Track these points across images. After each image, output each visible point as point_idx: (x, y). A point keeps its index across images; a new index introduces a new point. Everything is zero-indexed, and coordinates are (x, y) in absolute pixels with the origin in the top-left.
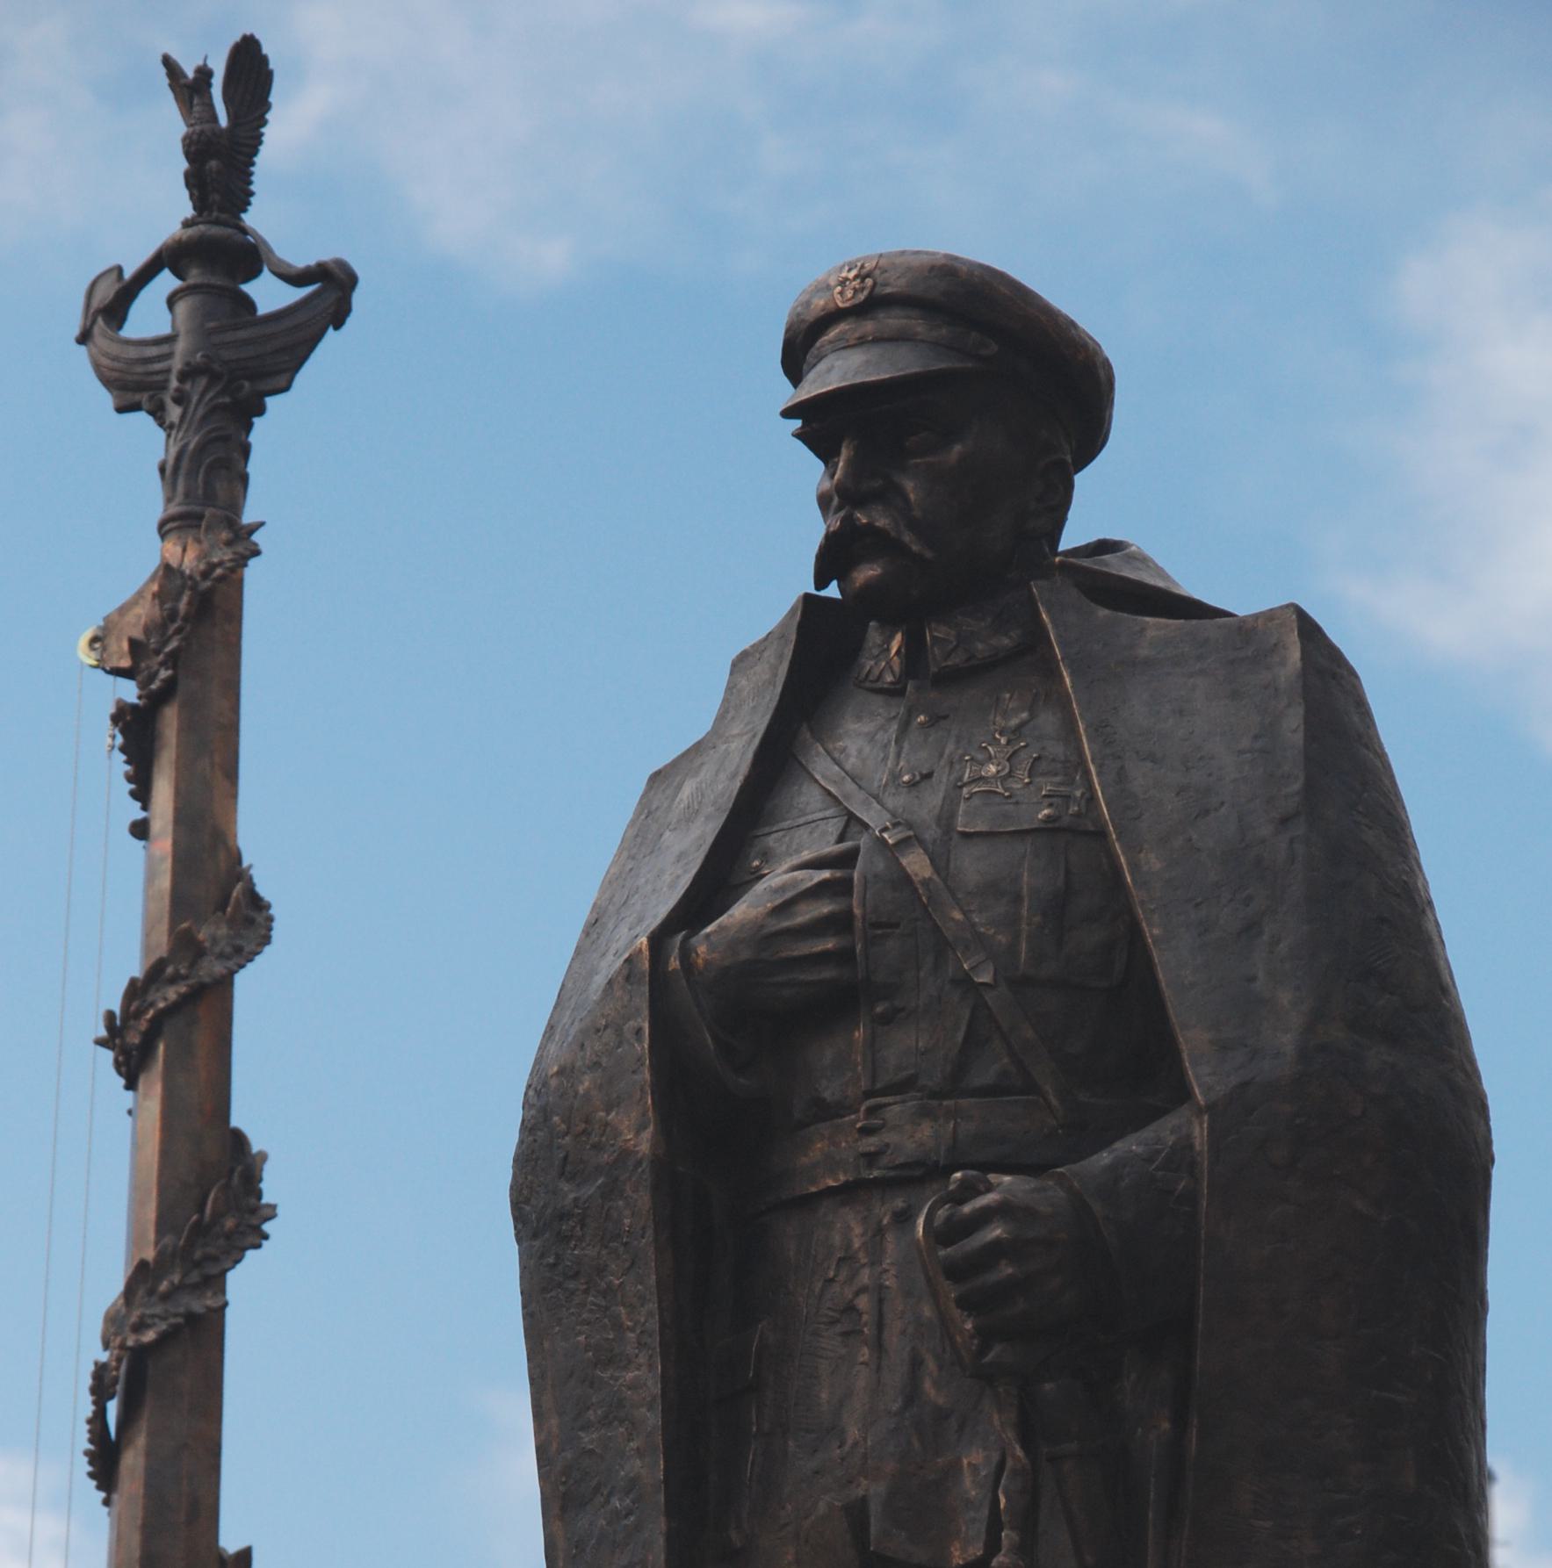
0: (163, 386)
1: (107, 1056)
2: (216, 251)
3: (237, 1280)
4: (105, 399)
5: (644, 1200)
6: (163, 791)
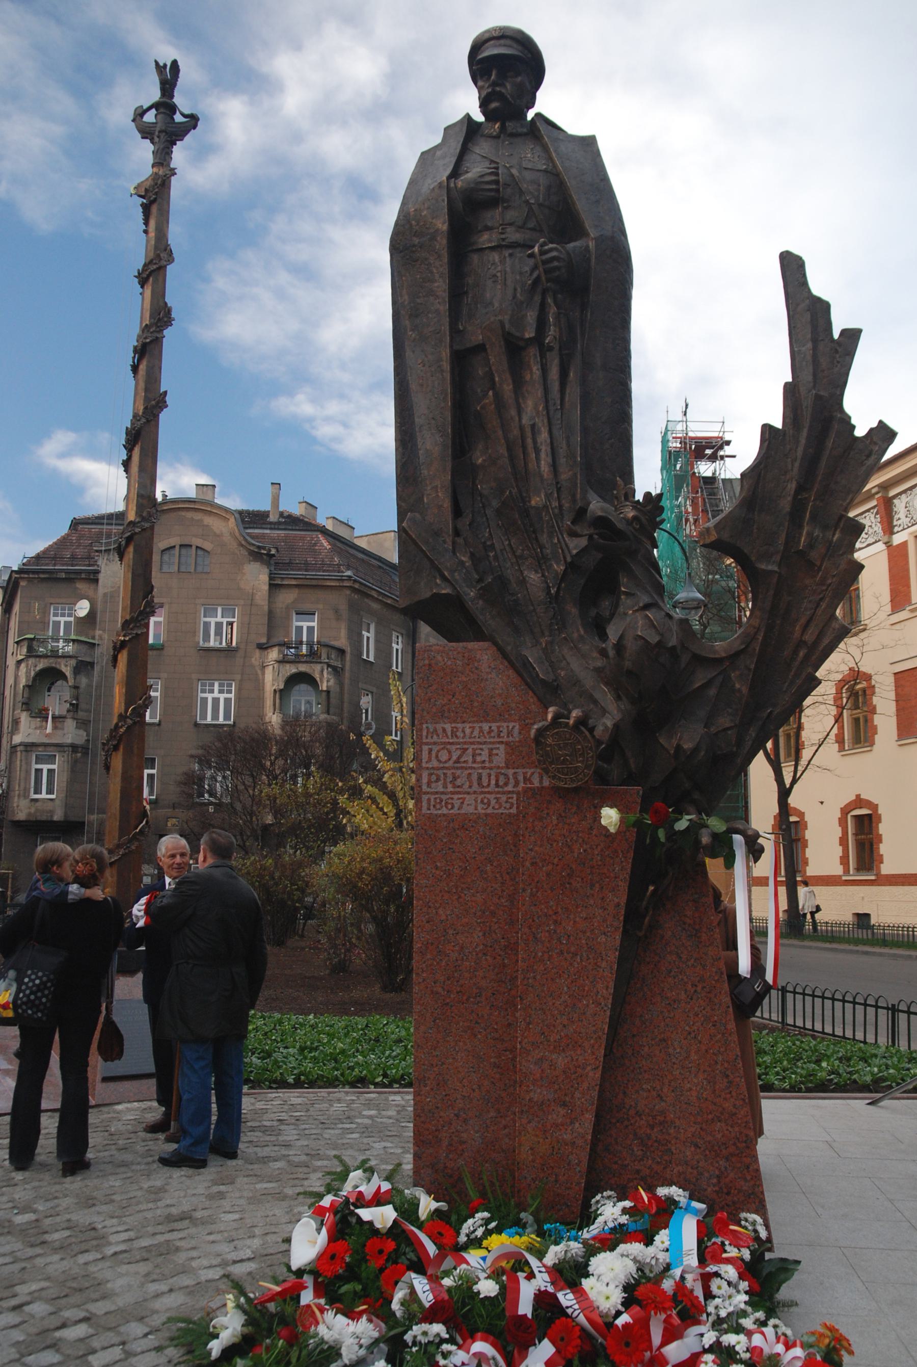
0: (153, 134)
1: (136, 280)
2: (166, 106)
3: (165, 332)
4: (139, 136)
5: (445, 242)
6: (152, 223)
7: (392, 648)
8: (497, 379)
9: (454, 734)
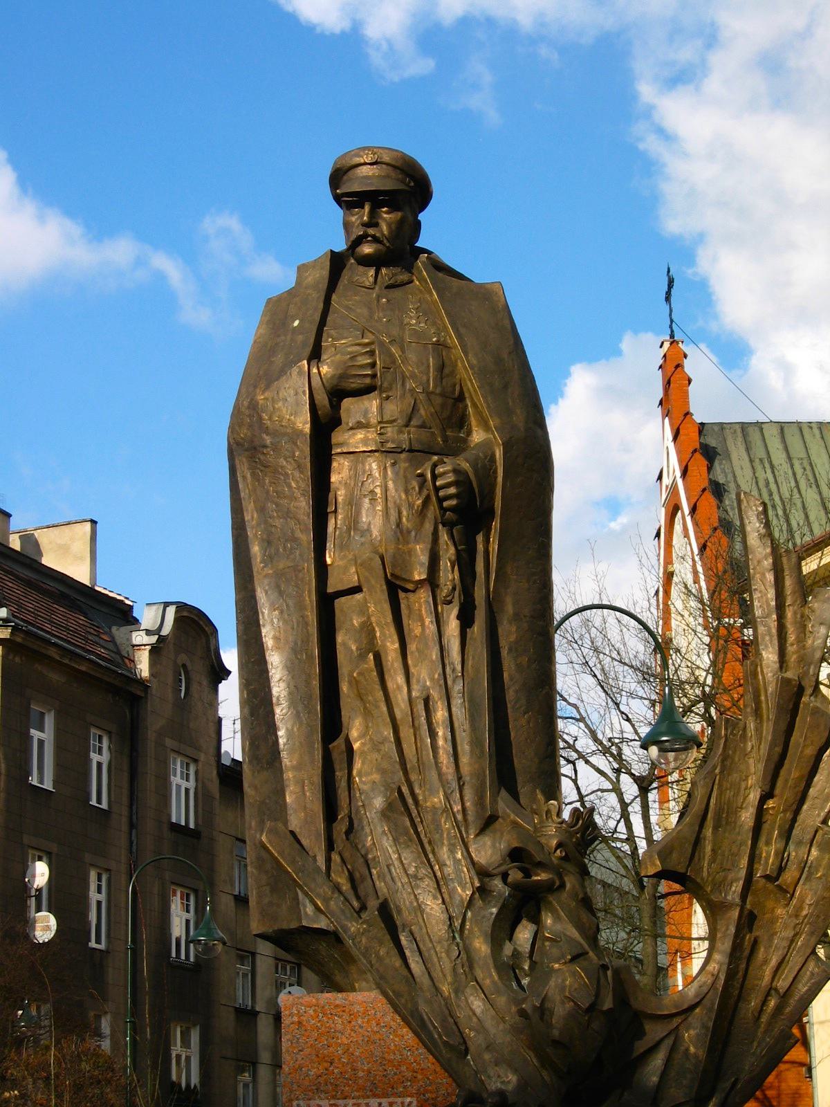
7: (88, 761)
8: (378, 634)
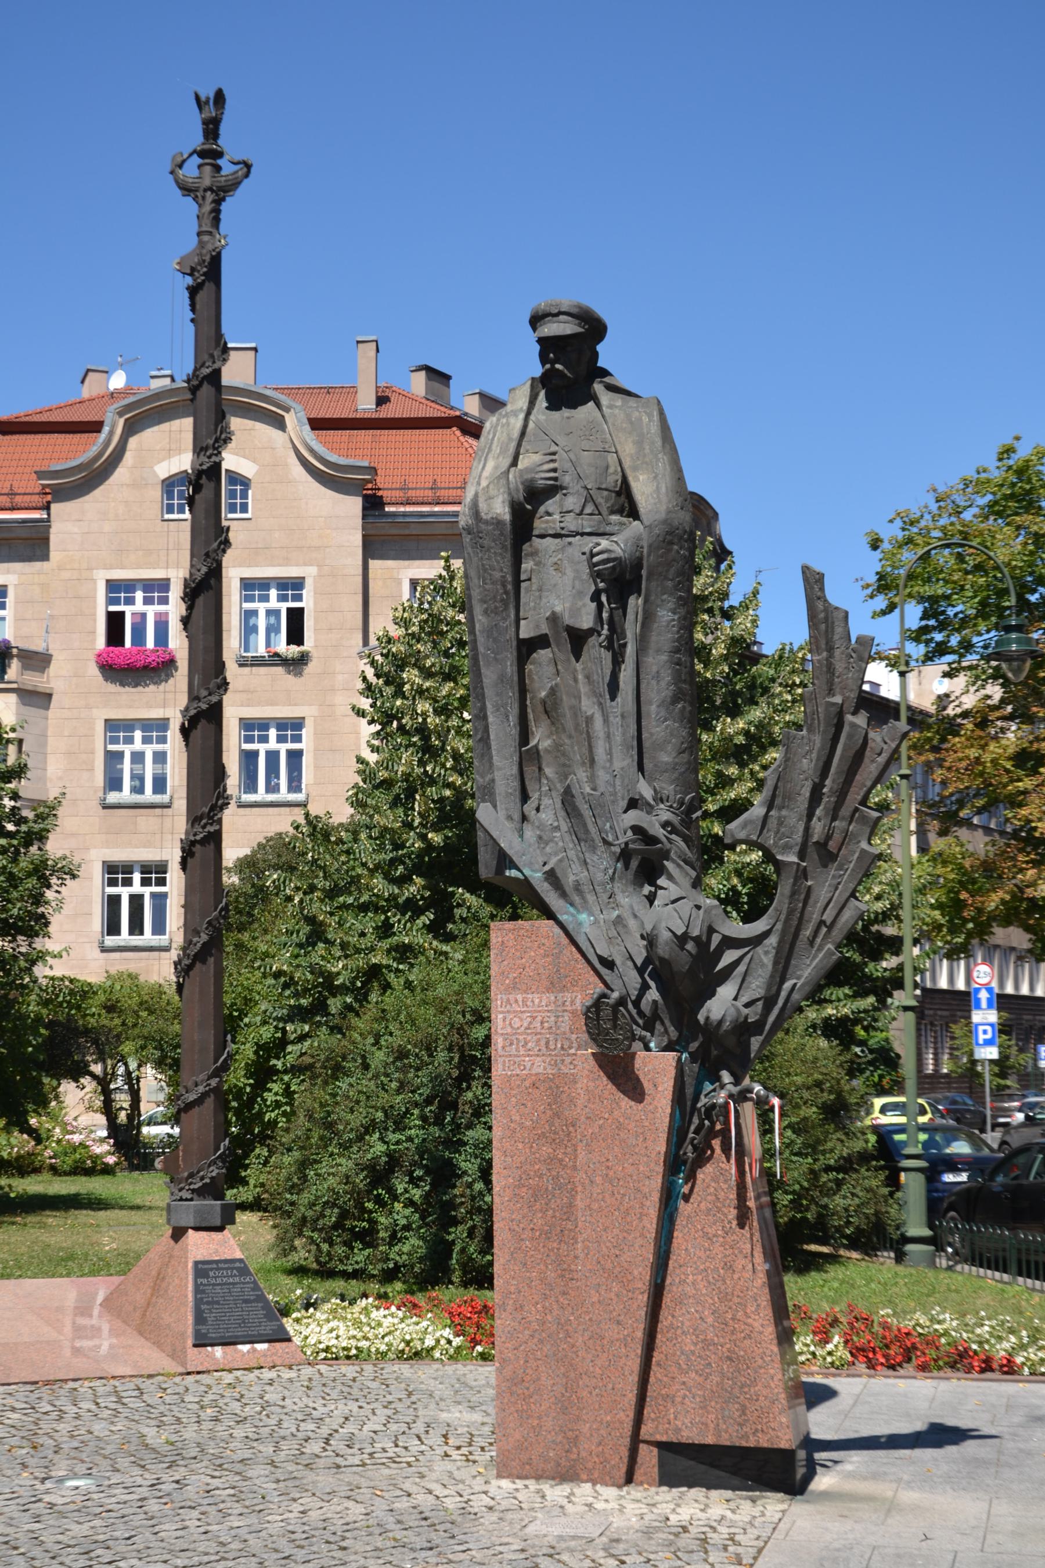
9: (525, 1004)
